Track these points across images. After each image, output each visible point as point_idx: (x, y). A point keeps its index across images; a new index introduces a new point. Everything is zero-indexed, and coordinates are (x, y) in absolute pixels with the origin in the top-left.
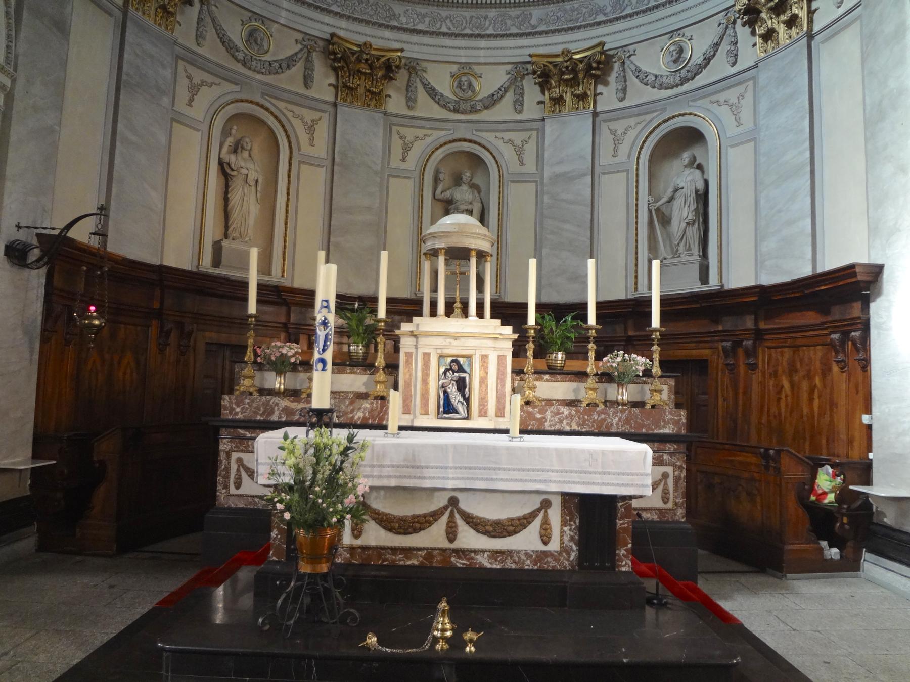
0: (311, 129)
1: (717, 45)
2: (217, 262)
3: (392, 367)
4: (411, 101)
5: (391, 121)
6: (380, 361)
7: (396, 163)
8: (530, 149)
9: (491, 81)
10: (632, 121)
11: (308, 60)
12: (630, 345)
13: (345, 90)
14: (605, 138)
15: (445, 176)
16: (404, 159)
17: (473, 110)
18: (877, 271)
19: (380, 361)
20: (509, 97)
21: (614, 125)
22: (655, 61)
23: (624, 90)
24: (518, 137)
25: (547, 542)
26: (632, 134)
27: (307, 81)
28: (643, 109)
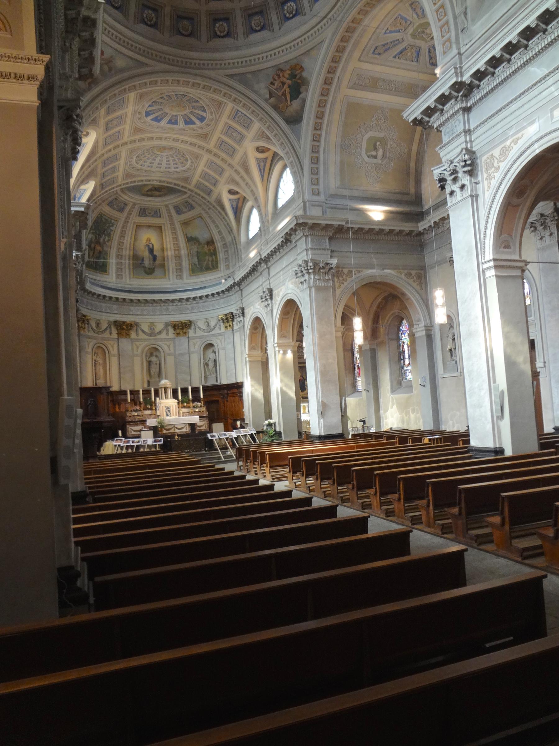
0: (113, 347)
1: (216, 325)
3: (156, 409)
4: (137, 335)
5: (133, 341)
6: (154, 408)
7: (135, 352)
9: (159, 327)
10: (198, 340)
11: (110, 328)
13: (119, 334)
14: (191, 343)
15: (148, 355)
16: (137, 351)
17: (155, 336)
18: (242, 383)
19: (154, 408)
20: (165, 332)
21: (194, 341)
22: (201, 324)
23: (195, 332)
24: (168, 343)
25: (187, 430)
26: (198, 343)
27: (111, 333)
28: (200, 337)
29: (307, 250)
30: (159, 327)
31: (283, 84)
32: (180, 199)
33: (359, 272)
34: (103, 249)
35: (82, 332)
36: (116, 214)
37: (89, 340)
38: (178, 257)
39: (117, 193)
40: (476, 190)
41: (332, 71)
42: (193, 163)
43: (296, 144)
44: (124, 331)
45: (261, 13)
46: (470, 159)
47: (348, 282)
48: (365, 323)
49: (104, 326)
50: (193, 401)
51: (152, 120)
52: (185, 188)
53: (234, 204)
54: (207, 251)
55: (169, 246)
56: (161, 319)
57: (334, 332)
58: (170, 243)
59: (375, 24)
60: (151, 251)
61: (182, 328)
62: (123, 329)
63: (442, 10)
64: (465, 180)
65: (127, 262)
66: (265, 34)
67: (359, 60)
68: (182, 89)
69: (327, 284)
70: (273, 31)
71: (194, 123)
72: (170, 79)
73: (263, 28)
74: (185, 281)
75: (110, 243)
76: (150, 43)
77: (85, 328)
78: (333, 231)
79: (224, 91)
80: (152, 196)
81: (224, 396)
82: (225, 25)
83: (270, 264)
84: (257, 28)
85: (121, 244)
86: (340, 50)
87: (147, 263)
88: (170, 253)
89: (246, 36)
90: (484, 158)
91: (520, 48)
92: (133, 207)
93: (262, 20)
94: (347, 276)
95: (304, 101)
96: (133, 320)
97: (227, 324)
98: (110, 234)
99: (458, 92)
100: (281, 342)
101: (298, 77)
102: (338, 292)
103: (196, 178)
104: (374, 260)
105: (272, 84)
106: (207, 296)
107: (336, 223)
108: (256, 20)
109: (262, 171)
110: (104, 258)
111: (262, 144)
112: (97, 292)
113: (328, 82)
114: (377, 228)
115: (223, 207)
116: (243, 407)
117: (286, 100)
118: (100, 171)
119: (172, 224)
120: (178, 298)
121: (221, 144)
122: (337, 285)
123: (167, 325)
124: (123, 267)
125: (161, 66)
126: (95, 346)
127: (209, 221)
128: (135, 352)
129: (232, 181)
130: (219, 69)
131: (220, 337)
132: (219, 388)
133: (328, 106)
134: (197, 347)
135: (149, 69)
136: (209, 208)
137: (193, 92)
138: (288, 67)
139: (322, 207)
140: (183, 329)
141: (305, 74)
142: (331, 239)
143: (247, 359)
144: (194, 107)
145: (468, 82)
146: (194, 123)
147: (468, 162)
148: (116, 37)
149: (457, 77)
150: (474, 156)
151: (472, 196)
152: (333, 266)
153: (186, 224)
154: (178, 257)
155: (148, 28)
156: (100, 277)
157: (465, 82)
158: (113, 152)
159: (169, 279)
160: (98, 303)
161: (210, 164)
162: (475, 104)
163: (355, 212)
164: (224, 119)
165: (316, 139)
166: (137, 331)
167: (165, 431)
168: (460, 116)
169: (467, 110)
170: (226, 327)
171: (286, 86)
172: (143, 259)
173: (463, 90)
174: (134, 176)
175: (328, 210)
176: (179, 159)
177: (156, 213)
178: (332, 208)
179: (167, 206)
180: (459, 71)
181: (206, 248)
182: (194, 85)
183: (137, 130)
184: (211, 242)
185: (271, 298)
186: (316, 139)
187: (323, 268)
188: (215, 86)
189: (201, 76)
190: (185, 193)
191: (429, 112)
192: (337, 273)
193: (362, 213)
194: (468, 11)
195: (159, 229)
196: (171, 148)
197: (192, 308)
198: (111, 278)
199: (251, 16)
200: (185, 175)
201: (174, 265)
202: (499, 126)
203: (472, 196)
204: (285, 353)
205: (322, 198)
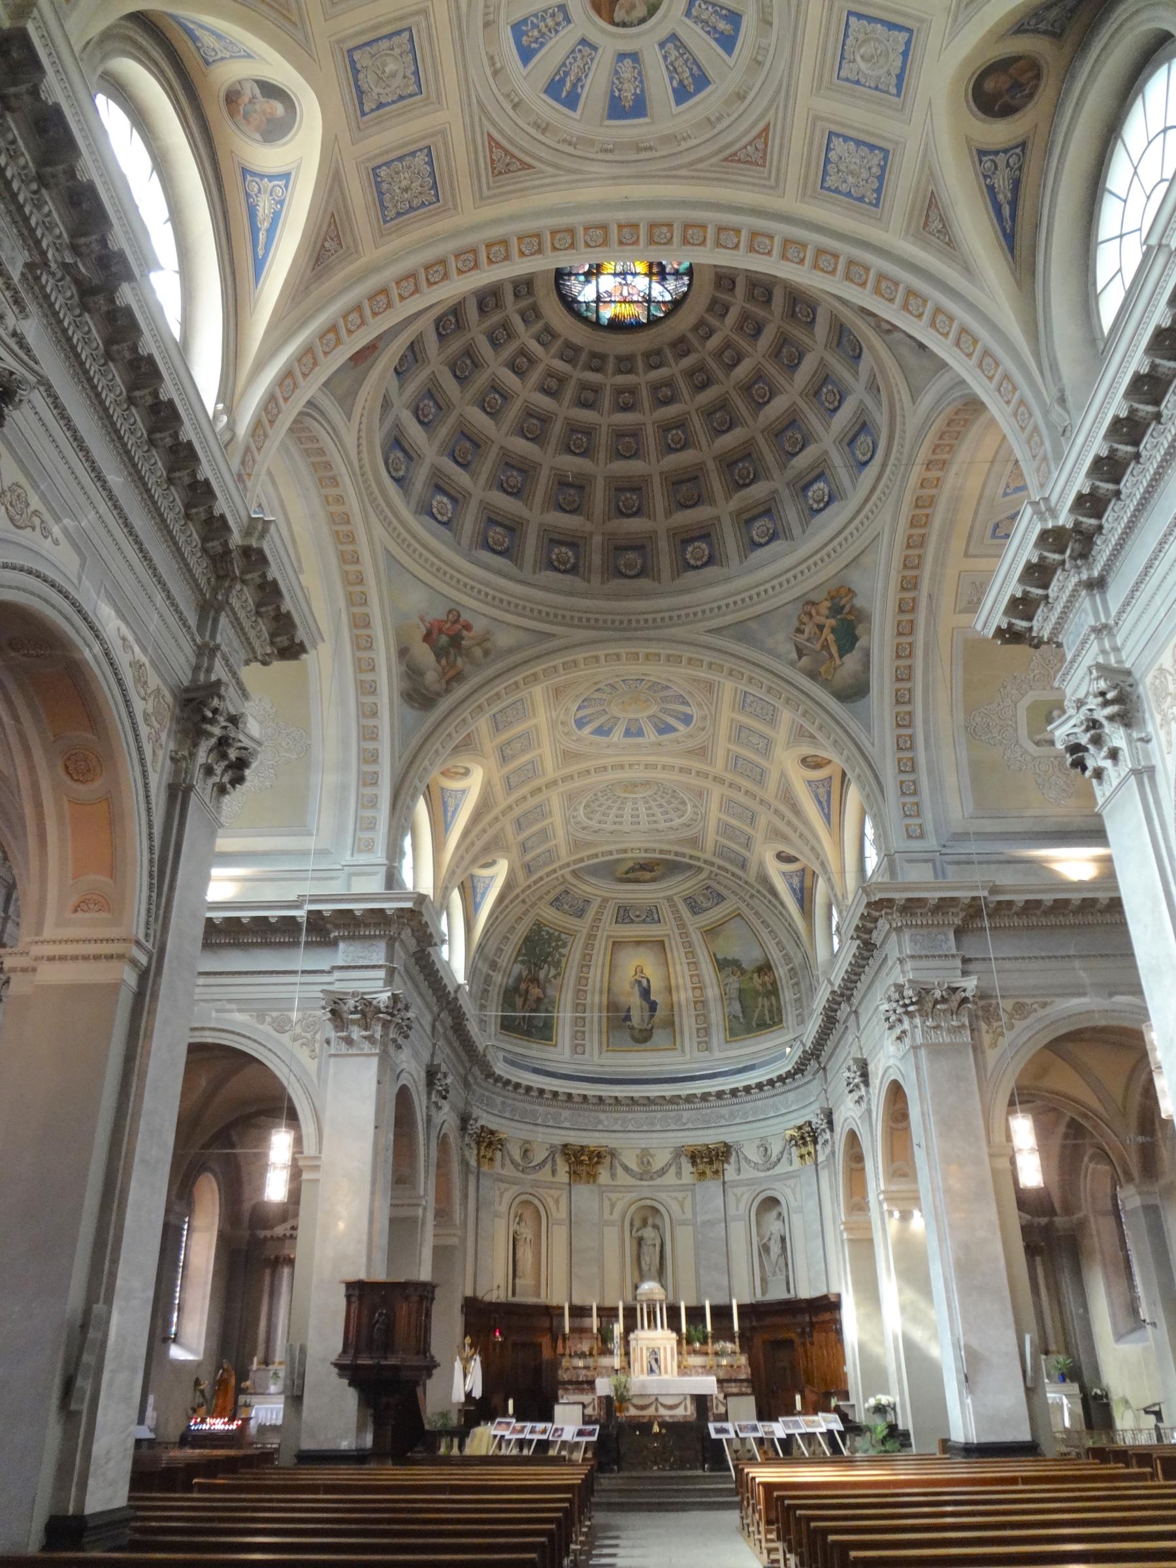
0: (557, 1202)
2: (514, 1294)
4: (613, 1176)
7: (607, 1216)
8: (688, 1203)
9: (661, 1158)
10: (744, 1189)
11: (554, 1160)
12: (725, 1339)
13: (574, 1174)
15: (637, 1223)
17: (652, 1178)
18: (839, 1296)
20: (673, 1170)
22: (752, 1153)
24: (680, 1195)
25: (686, 1411)
26: (745, 1197)
27: (554, 1172)
28: (752, 1182)
29: (901, 961)
30: (661, 1158)
31: (821, 627)
32: (692, 882)
33: (1044, 1005)
34: (544, 992)
35: (485, 1168)
36: (571, 922)
37: (503, 1186)
38: (701, 1004)
39: (565, 881)
40: (1147, 755)
41: (910, 584)
42: (695, 806)
43: (863, 737)
44: (584, 1168)
45: (767, 512)
46: (1115, 687)
47: (1016, 1031)
48: (1043, 1133)
49: (539, 1155)
50: (716, 1338)
51: (594, 732)
52: (699, 859)
53: (796, 881)
54: (760, 988)
55: (680, 981)
56: (663, 1141)
57: (987, 1159)
58: (686, 977)
59: (973, 485)
60: (646, 993)
61: (711, 1159)
62: (581, 1163)
63: (1022, 409)
64: (1117, 737)
65: (595, 1017)
66: (776, 546)
67: (967, 555)
68: (635, 669)
69: (958, 1040)
70: (793, 539)
71: (674, 730)
72: (601, 653)
73: (773, 537)
74: (717, 1054)
75: (559, 980)
76: (561, 600)
77: (491, 1159)
78: (962, 914)
79: (707, 659)
80: (637, 881)
81: (803, 1332)
82: (704, 546)
83: (855, 1001)
84: (763, 541)
85: (583, 981)
86: (916, 543)
87: (636, 1020)
88: (684, 996)
89: (744, 556)
90: (1149, 680)
91: (1149, 425)
92: (602, 906)
93: (770, 525)
94: (1011, 1017)
95: (867, 654)
96: (604, 1142)
97: (804, 1151)
98: (559, 962)
99: (1062, 552)
100: (894, 1188)
101: (847, 609)
102: (991, 1056)
103: (711, 838)
104: (1082, 974)
105: (799, 631)
106: (760, 1086)
107: (964, 895)
108: (759, 528)
109: (825, 806)
110: (547, 1011)
111: (807, 750)
112: (524, 1083)
113: (906, 608)
114: (1076, 897)
115: (774, 892)
116: (843, 1362)
117: (831, 656)
118: (512, 837)
119: (685, 934)
120: (698, 1092)
121: (736, 761)
122: (987, 1039)
123: (678, 1153)
124: (587, 1029)
125: (580, 634)
126: (518, 1200)
127: (756, 922)
128: (607, 1216)
129: (777, 834)
130: (693, 622)
131: (791, 1182)
132: (792, 1307)
133: (919, 653)
134: (742, 1206)
135: (556, 643)
136: (752, 896)
137: (656, 672)
138: (825, 595)
139: (932, 861)
140: (711, 1163)
141: (859, 602)
142: (959, 932)
143: (845, 1236)
144: (665, 700)
145: (1070, 525)
146: (674, 730)
147: (1110, 696)
148: (494, 598)
149: (1042, 519)
150: (1130, 680)
151: (1136, 772)
152: (969, 994)
153: (711, 933)
154: (701, 1004)
155: (560, 576)
156: (535, 1051)
157: (1063, 528)
158: (532, 802)
159: (683, 1051)
160: (528, 1107)
161: (728, 805)
162: (1108, 567)
163: (1019, 866)
164: (726, 714)
165: (904, 722)
166: (612, 1166)
167: (633, 1412)
168: (1085, 601)
169: (1098, 585)
170: (802, 1157)
171: (826, 631)
172: (629, 1010)
173: (1071, 543)
174: (589, 844)
175: (950, 869)
176: (670, 803)
177: (651, 915)
178: (958, 863)
179: (669, 899)
180: (1043, 507)
181: (757, 980)
182: (647, 657)
183: (568, 756)
184: (765, 968)
185: (866, 1083)
186: (904, 722)
187: (944, 1000)
188: (687, 653)
189: (659, 640)
190: (700, 869)
191: (1023, 606)
192: (980, 1010)
193: (1037, 866)
194: (1067, 393)
195: (660, 945)
196: (646, 783)
197: (732, 1115)
198: (559, 1053)
199: (749, 522)
200: (688, 833)
201: (693, 1020)
202: (1158, 600)
203: (1136, 772)
204: (906, 1216)
205: (931, 843)
